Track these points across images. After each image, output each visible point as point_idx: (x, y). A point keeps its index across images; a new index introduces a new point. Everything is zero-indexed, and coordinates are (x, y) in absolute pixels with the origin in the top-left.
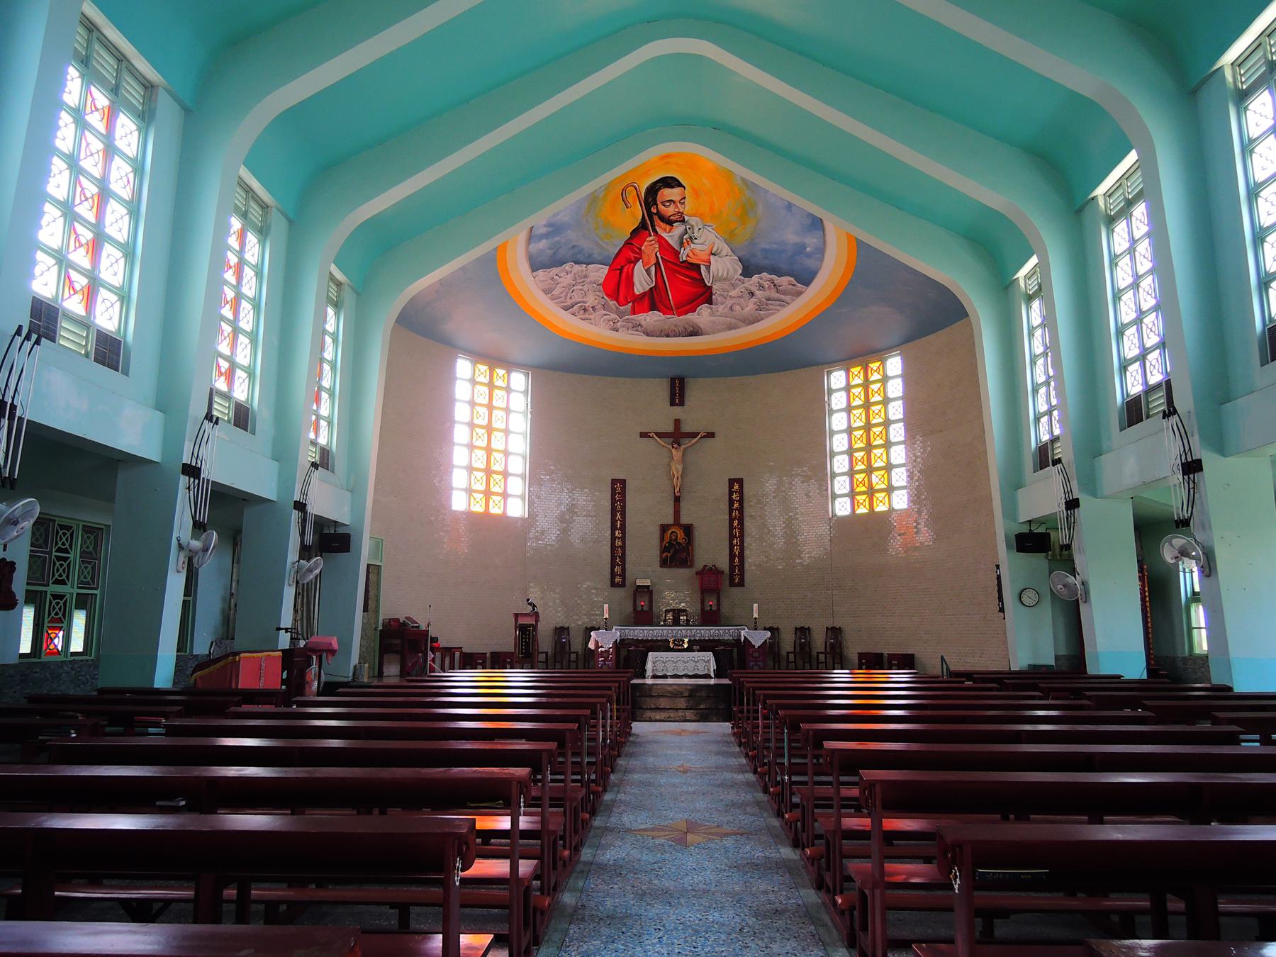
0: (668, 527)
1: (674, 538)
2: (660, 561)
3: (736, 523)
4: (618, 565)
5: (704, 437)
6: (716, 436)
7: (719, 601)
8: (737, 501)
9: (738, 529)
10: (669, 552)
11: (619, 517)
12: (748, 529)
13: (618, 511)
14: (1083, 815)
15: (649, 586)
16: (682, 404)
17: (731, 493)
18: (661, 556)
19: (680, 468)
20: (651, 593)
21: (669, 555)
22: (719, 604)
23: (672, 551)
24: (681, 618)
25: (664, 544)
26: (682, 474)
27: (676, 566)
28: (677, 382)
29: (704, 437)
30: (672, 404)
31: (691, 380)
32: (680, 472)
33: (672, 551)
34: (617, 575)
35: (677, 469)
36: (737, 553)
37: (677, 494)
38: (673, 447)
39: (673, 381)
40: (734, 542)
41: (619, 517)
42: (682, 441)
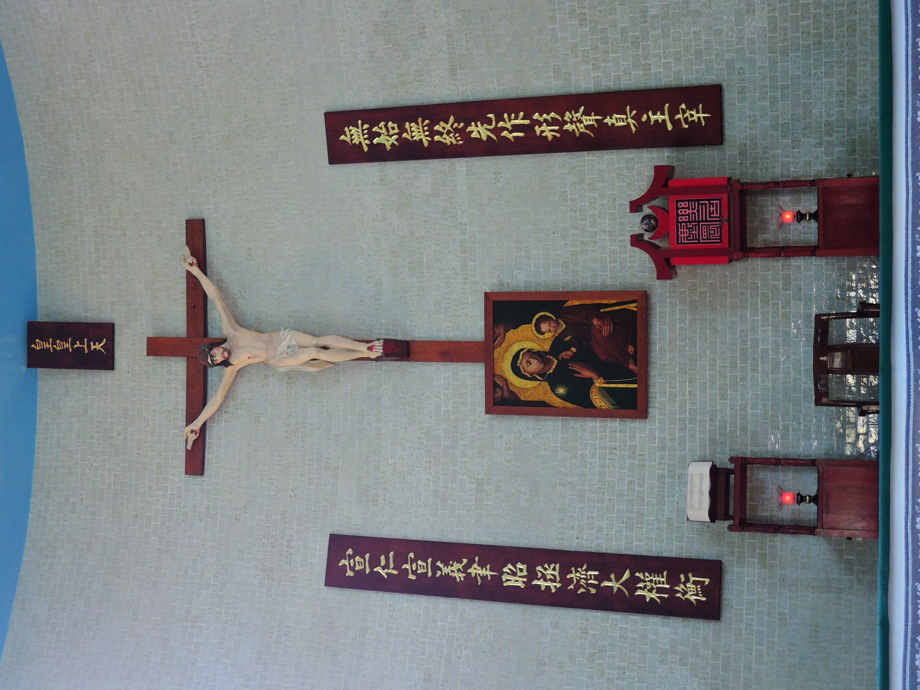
0: (496, 386)
1: (535, 366)
2: (623, 417)
3: (479, 131)
4: (632, 584)
5: (203, 266)
6: (198, 216)
7: (775, 187)
8: (402, 130)
9: (499, 118)
10: (590, 382)
11: (454, 570)
12: (496, 93)
13: (435, 569)
14: (596, 571)
15: (714, 471)
16: (106, 331)
17: (377, 154)
18: (604, 414)
19: (289, 338)
20: (743, 464)
21: (599, 383)
22: (794, 185)
23: (587, 374)
24: (852, 336)
25: (557, 402)
26: (314, 334)
27: (642, 357)
28: (40, 345)
29: (203, 266)
30: (105, 361)
31: (41, 301)
32: (307, 340)
33: (587, 374)
34: (672, 592)
35: (293, 350)
36: (589, 120)
37: (378, 351)
38: (226, 363)
39: (36, 360)
40: (548, 132)
41: (454, 570)
42: (213, 333)
